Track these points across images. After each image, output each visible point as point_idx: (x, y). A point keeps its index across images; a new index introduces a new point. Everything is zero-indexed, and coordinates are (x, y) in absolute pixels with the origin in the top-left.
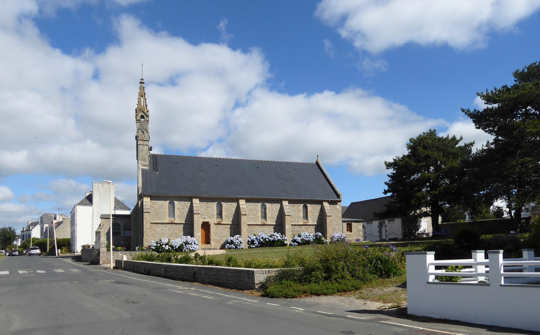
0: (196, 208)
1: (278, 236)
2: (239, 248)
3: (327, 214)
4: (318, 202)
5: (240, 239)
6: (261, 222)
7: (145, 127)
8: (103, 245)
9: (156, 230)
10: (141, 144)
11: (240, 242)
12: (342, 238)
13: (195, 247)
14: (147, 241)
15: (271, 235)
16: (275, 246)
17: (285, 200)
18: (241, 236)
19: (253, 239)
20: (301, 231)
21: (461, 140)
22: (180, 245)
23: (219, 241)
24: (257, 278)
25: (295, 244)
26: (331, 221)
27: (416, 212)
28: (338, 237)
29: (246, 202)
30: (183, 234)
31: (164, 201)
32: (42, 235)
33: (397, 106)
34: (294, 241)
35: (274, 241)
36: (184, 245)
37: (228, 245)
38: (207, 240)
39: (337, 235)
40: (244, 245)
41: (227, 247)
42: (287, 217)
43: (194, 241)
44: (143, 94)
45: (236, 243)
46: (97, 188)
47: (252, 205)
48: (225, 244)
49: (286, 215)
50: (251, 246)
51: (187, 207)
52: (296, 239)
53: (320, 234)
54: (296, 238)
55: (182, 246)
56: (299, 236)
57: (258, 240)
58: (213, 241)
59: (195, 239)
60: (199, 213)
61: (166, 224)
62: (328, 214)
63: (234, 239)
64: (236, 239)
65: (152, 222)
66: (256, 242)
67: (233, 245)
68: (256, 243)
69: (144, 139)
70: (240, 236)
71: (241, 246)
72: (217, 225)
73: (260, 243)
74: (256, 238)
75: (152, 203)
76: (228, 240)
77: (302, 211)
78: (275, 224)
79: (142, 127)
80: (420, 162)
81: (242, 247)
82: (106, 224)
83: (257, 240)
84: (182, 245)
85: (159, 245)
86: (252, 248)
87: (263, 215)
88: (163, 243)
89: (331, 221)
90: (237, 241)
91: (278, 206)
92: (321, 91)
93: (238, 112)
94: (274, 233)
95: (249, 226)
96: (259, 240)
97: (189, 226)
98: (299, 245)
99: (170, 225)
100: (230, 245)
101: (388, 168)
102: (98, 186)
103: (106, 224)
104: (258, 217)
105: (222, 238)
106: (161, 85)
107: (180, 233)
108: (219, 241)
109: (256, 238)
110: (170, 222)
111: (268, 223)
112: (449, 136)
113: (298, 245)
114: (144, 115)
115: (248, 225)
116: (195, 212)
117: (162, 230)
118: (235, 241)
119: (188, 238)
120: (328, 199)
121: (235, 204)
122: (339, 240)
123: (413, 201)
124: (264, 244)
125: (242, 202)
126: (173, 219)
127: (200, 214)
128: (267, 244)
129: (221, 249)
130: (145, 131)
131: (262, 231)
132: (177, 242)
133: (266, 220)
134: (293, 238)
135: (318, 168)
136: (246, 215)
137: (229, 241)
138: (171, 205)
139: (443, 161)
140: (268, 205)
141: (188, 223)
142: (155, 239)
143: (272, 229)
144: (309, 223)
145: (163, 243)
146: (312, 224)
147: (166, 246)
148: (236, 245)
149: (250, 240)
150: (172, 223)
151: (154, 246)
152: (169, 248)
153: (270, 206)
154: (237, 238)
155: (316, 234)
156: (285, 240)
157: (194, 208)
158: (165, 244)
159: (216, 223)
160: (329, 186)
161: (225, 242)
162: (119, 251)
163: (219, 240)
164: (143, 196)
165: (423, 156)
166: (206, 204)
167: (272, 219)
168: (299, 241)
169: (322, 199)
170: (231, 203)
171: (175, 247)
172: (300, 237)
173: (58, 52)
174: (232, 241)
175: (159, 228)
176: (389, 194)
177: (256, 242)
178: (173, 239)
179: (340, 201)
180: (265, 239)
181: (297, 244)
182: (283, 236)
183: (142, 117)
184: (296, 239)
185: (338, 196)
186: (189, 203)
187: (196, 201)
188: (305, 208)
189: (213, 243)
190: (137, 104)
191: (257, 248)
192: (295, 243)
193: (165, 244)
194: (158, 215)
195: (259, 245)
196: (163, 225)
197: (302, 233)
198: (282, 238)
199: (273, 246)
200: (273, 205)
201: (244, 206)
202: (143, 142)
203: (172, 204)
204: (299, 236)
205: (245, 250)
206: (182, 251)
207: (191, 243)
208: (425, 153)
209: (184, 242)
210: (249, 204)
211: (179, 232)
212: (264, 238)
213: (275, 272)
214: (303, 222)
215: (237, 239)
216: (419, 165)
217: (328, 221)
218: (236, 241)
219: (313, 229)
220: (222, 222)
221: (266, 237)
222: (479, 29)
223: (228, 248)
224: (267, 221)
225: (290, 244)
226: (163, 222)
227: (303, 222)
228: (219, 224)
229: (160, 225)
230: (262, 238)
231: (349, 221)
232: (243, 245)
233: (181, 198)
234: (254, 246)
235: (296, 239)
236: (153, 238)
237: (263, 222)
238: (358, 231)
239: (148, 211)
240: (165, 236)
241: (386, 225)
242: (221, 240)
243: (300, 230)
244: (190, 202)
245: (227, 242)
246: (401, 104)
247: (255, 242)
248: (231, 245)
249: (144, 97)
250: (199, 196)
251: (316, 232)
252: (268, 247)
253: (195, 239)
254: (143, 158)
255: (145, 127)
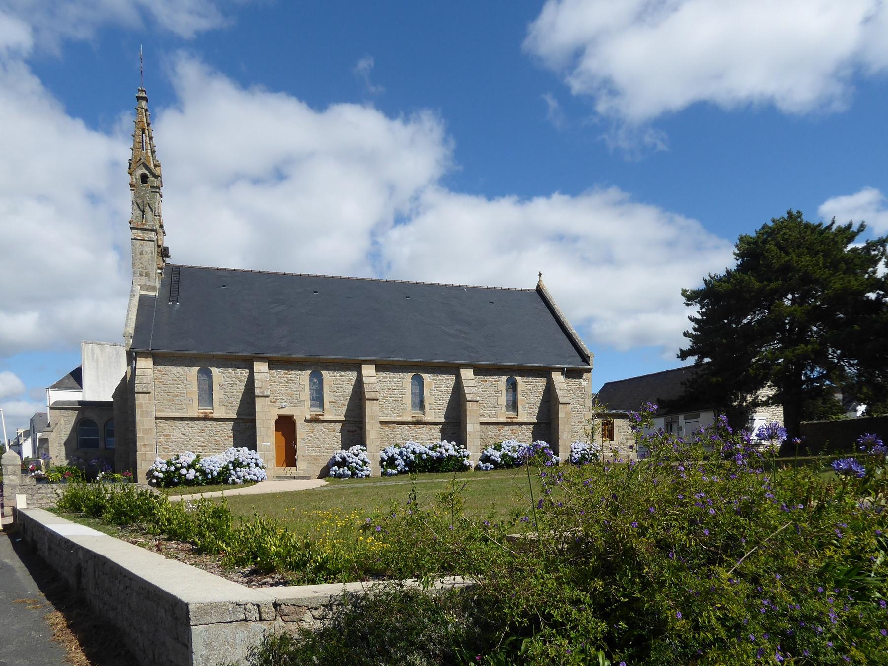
0: (260, 382)
1: (449, 448)
2: (359, 475)
3: (560, 398)
4: (540, 372)
5: (363, 455)
6: (413, 417)
7: (148, 199)
8: (10, 468)
9: (169, 435)
10: (139, 238)
11: (363, 461)
12: (592, 452)
13: (258, 474)
14: (145, 460)
15: (433, 446)
16: (442, 471)
17: (467, 366)
18: (365, 448)
19: (393, 455)
20: (501, 437)
21: (861, 233)
22: (221, 469)
23: (316, 460)
24: (208, 645)
25: (487, 467)
26: (568, 414)
27: (744, 399)
28: (584, 450)
29: (376, 372)
30: (232, 443)
31: (186, 368)
32: (34, 452)
33: (681, 220)
34: (486, 459)
35: (440, 459)
36: (232, 468)
37: (336, 468)
38: (290, 459)
39: (581, 446)
40: (373, 469)
41: (334, 473)
42: (469, 406)
43: (256, 460)
44: (146, 125)
45: (354, 464)
46: (90, 354)
47: (392, 378)
48: (330, 465)
49: (468, 399)
50: (389, 470)
51: (240, 381)
52: (491, 456)
53: (544, 444)
54: (490, 451)
55: (226, 471)
56: (498, 448)
57: (405, 458)
58: (301, 460)
59: (257, 456)
60: (266, 394)
61: (192, 419)
62: (562, 400)
63: (350, 454)
64: (353, 455)
65: (159, 415)
66: (400, 462)
67: (346, 468)
68: (399, 464)
69: (145, 227)
70: (362, 448)
71: (365, 471)
72: (313, 424)
73: (409, 464)
74: (400, 454)
75: (158, 371)
76: (335, 457)
77: (504, 392)
78: (444, 420)
79: (140, 197)
80: (770, 281)
81: (368, 473)
82: (62, 422)
83: (402, 457)
84: (226, 468)
85: (173, 468)
86: (391, 475)
87: (418, 401)
88: (181, 464)
89: (568, 413)
90: (356, 459)
91: (450, 380)
92: (546, 193)
93: (396, 234)
94: (442, 440)
95: (384, 427)
96: (407, 458)
97: (247, 424)
98: (496, 469)
99: (202, 423)
100: (339, 469)
101: (690, 303)
102: (92, 350)
103: (62, 422)
104: (405, 405)
105: (323, 453)
106: (256, 181)
107: (226, 442)
108: (316, 459)
109: (400, 454)
110: (201, 416)
111: (427, 419)
112: (836, 222)
113: (495, 468)
114: (148, 174)
115: (381, 423)
116: (257, 392)
117: (184, 434)
118: (350, 460)
119: (241, 452)
120: (562, 366)
121: (353, 376)
122: (586, 456)
123: (753, 369)
124: (419, 465)
125: (368, 371)
126: (208, 408)
127: (268, 396)
128: (425, 466)
129: (320, 477)
130: (147, 208)
131: (415, 438)
132: (215, 462)
133: (422, 413)
134: (483, 453)
135: (540, 300)
136: (377, 399)
137: (339, 459)
138: (205, 378)
139: (824, 277)
140: (427, 378)
141: (243, 419)
142: (169, 455)
143: (436, 432)
144: (520, 419)
145: (181, 464)
146: (526, 421)
147: (188, 471)
148: (354, 469)
149: (386, 458)
150: (206, 419)
151: (162, 472)
152: (195, 476)
153: (433, 380)
154: (356, 453)
155: (535, 443)
156: (464, 456)
157: (256, 382)
158: (186, 465)
159: (309, 417)
160: (565, 337)
161: (329, 462)
162: (52, 482)
163: (315, 457)
164: (134, 354)
165: (777, 266)
166: (286, 374)
167: (436, 412)
168: (497, 459)
169: (549, 365)
170: (343, 373)
171: (211, 474)
172: (499, 450)
173: (79, 125)
174: (344, 459)
175: (176, 431)
176: (691, 361)
177: (400, 462)
178: (209, 456)
179: (589, 371)
180: (421, 454)
181: (493, 466)
182: (460, 448)
183: (144, 178)
184: (489, 455)
185: (585, 358)
186: (246, 373)
187: (261, 368)
188: (512, 387)
189: (302, 465)
190: (132, 147)
191: (402, 476)
192: (488, 464)
193: (186, 465)
194: (173, 400)
195: (407, 469)
196: (185, 423)
197: (504, 442)
198: (459, 453)
199: (437, 471)
200: (440, 377)
201: (373, 380)
202: (143, 234)
203: (205, 373)
204: (498, 448)
205: (375, 480)
206: (225, 481)
207: (248, 464)
208: (784, 258)
209: (231, 462)
210: (385, 375)
211: (223, 438)
212: (418, 452)
213: (317, 613)
214: (507, 418)
215: (357, 456)
216: (768, 288)
217: (561, 415)
218: (354, 460)
219: (528, 432)
220: (323, 415)
221: (423, 449)
222: (835, 75)
223: (335, 475)
224: (426, 413)
225: (477, 465)
226: (185, 415)
227: (507, 418)
228: (315, 420)
229: (178, 423)
230: (414, 452)
231: (606, 415)
232: (370, 469)
233: (228, 361)
234: (394, 471)
235: (491, 456)
236: (163, 453)
237: (417, 415)
238: (627, 438)
239: (145, 390)
240: (190, 448)
241: (681, 427)
242: (320, 456)
243: (499, 436)
244: (247, 371)
245: (333, 462)
246: (688, 216)
247: (397, 463)
248: (342, 469)
249: (146, 131)
250: (269, 355)
251: (534, 440)
252: (427, 473)
253: (257, 456)
254: (144, 271)
255: (148, 199)
